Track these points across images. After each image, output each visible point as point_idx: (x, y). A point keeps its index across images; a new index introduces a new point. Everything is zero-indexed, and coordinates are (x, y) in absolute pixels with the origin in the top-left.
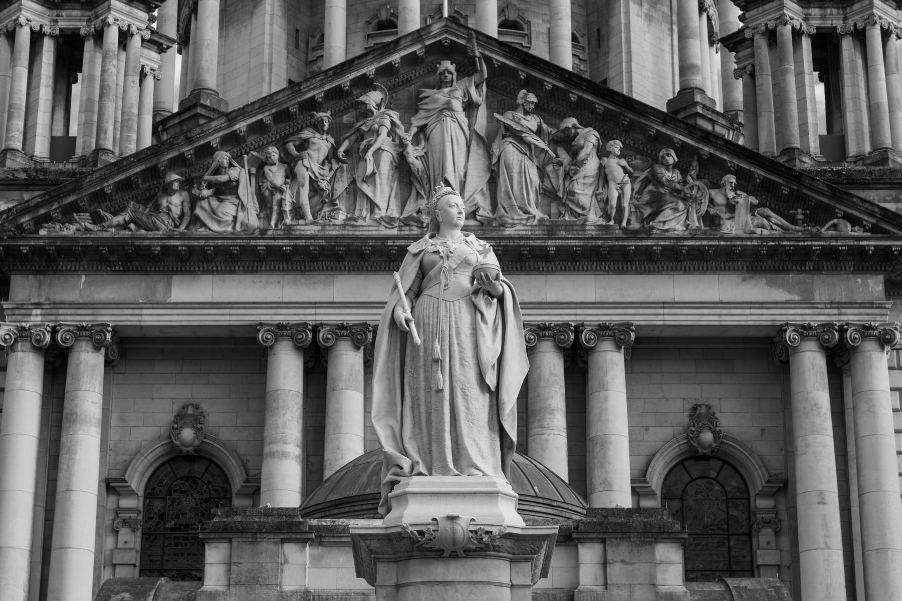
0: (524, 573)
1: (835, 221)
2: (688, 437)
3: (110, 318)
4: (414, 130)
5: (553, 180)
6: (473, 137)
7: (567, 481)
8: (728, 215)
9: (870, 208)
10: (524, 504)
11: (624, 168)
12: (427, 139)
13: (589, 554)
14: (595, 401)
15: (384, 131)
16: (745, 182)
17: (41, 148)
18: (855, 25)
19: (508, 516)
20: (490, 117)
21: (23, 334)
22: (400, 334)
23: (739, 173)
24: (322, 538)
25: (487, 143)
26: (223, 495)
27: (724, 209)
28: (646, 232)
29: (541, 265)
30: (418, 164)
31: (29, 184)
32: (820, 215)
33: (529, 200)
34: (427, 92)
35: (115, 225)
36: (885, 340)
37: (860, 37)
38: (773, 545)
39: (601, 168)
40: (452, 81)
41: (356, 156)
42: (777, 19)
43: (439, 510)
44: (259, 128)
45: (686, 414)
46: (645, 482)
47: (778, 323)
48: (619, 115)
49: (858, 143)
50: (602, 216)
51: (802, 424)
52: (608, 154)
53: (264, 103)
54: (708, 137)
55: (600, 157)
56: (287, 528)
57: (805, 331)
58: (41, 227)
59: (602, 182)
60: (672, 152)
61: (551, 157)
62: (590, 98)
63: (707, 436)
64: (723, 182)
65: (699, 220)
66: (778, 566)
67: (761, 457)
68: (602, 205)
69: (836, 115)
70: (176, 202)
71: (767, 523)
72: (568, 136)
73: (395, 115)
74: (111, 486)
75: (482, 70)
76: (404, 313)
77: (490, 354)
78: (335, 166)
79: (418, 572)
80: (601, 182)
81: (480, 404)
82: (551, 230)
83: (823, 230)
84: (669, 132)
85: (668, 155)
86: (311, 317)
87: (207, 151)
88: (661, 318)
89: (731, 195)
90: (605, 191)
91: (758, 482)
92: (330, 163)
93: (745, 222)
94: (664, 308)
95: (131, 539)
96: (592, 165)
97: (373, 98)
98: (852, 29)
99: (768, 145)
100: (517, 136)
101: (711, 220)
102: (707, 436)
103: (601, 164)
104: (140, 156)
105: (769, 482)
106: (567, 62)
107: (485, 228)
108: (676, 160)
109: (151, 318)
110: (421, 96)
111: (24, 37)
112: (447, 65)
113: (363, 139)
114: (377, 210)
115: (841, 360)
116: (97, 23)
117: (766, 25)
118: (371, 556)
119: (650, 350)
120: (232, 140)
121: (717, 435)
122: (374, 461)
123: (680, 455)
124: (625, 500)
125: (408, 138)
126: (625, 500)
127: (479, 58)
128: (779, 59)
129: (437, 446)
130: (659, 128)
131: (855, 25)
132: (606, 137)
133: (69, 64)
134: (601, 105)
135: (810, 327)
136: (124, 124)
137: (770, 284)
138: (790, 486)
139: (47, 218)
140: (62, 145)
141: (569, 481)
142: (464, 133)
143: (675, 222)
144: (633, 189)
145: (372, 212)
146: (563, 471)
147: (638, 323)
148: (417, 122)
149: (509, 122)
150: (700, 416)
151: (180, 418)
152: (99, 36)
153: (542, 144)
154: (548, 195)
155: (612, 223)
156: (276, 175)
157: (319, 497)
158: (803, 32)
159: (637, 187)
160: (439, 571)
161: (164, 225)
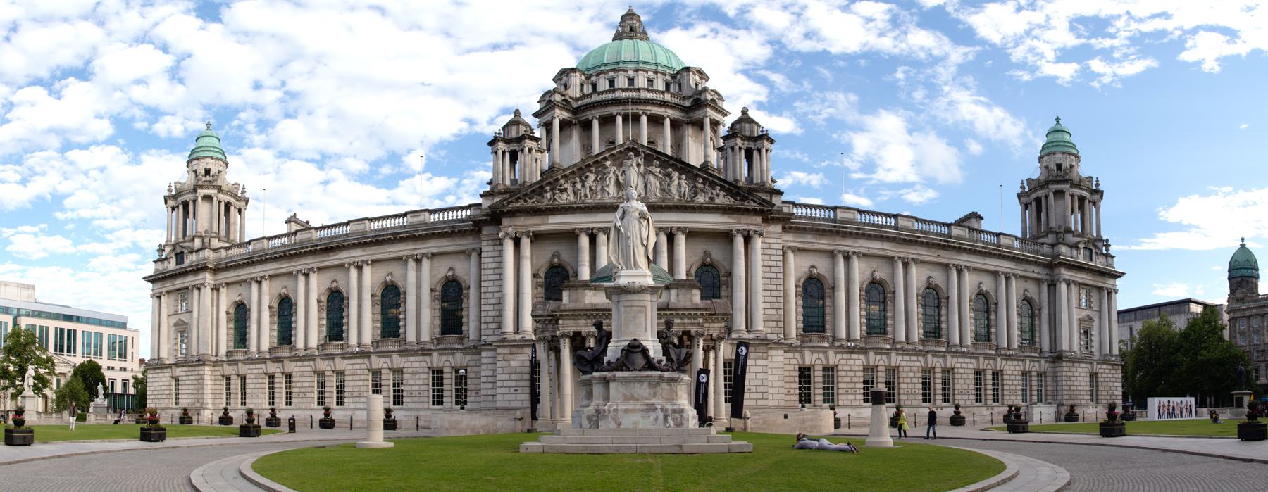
0: (655, 298)
3: (532, 229)
6: (639, 174)
9: (759, 198)
10: (655, 278)
13: (673, 292)
14: (676, 249)
16: (723, 188)
17: (508, 183)
19: (650, 282)
21: (507, 234)
22: (618, 230)
24: (596, 288)
25: (644, 176)
26: (567, 277)
28: (692, 201)
31: (505, 192)
32: (744, 199)
35: (531, 203)
36: (761, 235)
37: (759, 151)
41: (603, 179)
43: (630, 280)
44: (573, 173)
48: (685, 168)
49: (757, 180)
51: (735, 257)
53: (574, 166)
54: (712, 175)
56: (586, 286)
57: (738, 231)
59: (679, 186)
62: (677, 163)
70: (549, 195)
74: (535, 276)
76: (619, 224)
77: (645, 236)
79: (624, 297)
81: (642, 250)
82: (663, 201)
86: (591, 226)
87: (557, 180)
91: (722, 273)
93: (722, 199)
95: (542, 290)
96: (676, 182)
97: (608, 163)
99: (730, 179)
100: (653, 174)
101: (712, 199)
104: (537, 183)
106: (669, 153)
107: (643, 200)
109: (543, 228)
111: (500, 153)
115: (748, 239)
118: (610, 293)
119: (691, 235)
120: (565, 177)
122: (611, 266)
124: (684, 277)
126: (684, 277)
128: (734, 155)
129: (630, 263)
133: (514, 158)
136: (532, 173)
140: (514, 181)
143: (701, 199)
146: (666, 268)
150: (707, 254)
151: (553, 256)
152: (522, 150)
154: (663, 190)
156: (579, 186)
157: (595, 276)
160: (630, 297)
161: (546, 201)
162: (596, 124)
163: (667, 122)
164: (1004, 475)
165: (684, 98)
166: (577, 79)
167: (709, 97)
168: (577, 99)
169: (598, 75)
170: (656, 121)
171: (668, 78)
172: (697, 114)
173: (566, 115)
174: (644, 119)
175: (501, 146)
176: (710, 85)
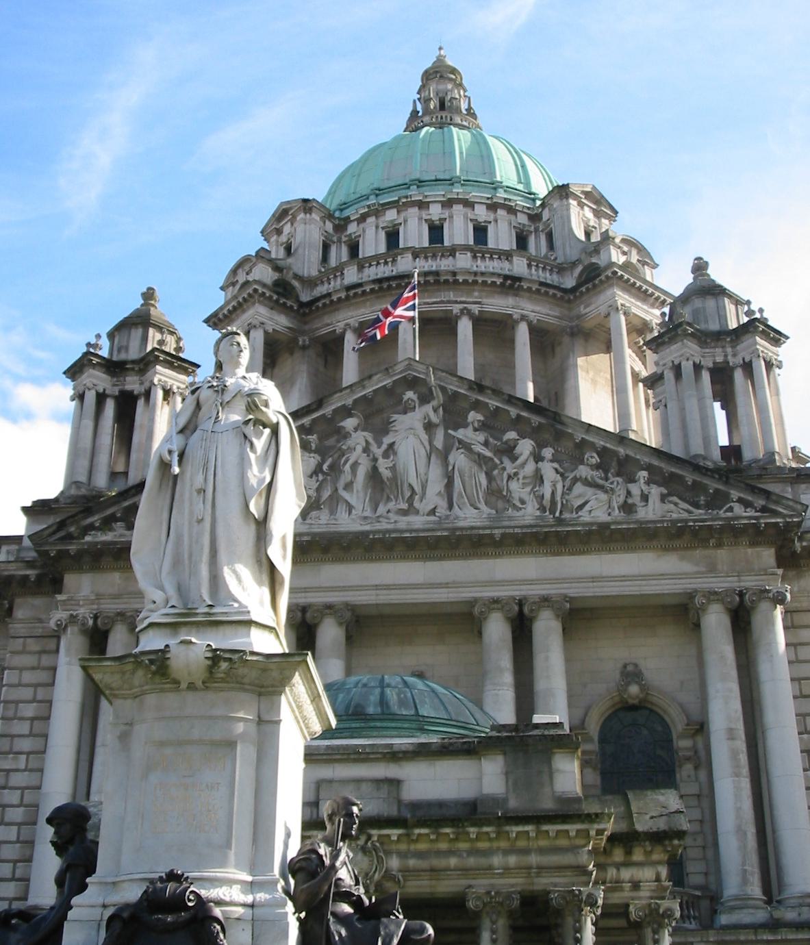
1: (732, 504)
2: (619, 690)
4: (384, 447)
5: (499, 482)
8: (643, 504)
11: (556, 470)
12: (395, 454)
15: (359, 449)
18: (744, 359)
20: (447, 435)
21: (73, 619)
23: (649, 468)
29: (490, 550)
30: (386, 473)
32: (718, 501)
33: (478, 498)
34: (395, 417)
37: (748, 368)
38: (693, 778)
39: (538, 470)
40: (415, 407)
46: (584, 729)
47: (689, 591)
50: (538, 509)
55: (537, 463)
57: (712, 595)
58: (86, 534)
60: (595, 455)
61: (496, 464)
64: (637, 477)
65: (619, 508)
66: (699, 796)
67: (681, 705)
68: (539, 500)
69: (734, 430)
71: (688, 759)
72: (510, 446)
73: (369, 436)
75: (438, 397)
78: (321, 477)
80: (538, 482)
83: (722, 511)
84: (591, 439)
85: (592, 457)
88: (592, 590)
92: (317, 476)
94: (593, 582)
96: (530, 468)
97: (350, 423)
98: (742, 362)
100: (466, 446)
101: (627, 508)
105: (688, 725)
108: (599, 461)
110: (391, 420)
112: (410, 395)
113: (344, 455)
114: (353, 511)
115: (742, 621)
116: (147, 385)
117: (673, 362)
119: (579, 617)
121: (643, 688)
123: (614, 706)
125: (378, 452)
127: (435, 387)
130: (584, 436)
131: (744, 359)
132: (540, 445)
135: (716, 593)
137: (682, 558)
138: (705, 727)
139: (91, 527)
142: (425, 447)
144: (564, 486)
145: (350, 513)
147: (572, 595)
148: (387, 440)
149: (461, 437)
152: (148, 394)
153: (488, 454)
155: (547, 513)
158: (702, 367)
159: (568, 483)
162: (350, 340)
163: (522, 334)
164: (584, 731)
165: (561, 269)
166: (308, 232)
167: (617, 257)
168: (310, 283)
169: (363, 219)
170: (494, 331)
171: (522, 219)
172: (593, 309)
173: (281, 322)
174: (465, 328)
175: (97, 379)
176: (619, 230)
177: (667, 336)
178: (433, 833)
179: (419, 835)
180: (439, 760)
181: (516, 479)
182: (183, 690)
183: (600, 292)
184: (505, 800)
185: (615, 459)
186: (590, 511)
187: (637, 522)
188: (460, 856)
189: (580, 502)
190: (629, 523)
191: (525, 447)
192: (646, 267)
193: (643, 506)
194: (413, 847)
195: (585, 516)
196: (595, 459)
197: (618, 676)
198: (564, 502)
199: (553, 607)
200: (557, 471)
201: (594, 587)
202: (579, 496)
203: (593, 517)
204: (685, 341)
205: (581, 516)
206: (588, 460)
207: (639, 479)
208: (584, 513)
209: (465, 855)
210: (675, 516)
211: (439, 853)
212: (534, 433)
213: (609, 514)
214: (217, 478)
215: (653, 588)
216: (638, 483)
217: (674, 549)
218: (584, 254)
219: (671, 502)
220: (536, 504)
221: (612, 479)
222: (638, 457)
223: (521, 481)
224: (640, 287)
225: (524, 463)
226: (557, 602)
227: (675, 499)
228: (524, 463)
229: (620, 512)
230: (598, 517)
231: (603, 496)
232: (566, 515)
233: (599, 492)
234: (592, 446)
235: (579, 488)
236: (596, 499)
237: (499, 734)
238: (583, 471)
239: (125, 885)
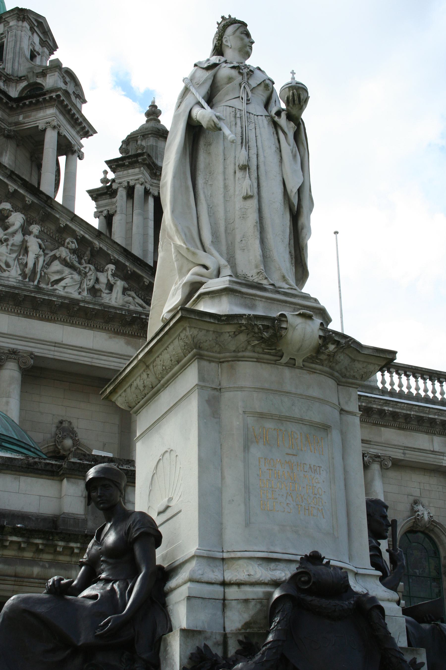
7: (18, 423)
8: (107, 291)
23: (116, 263)
27: (105, 286)
39: (24, 242)
42: (136, 180)
45: (54, 425)
50: (20, 275)
52: (30, 233)
55: (24, 235)
63: (68, 442)
65: (87, 290)
72: (3, 215)
80: (22, 252)
84: (74, 227)
85: (72, 242)
88: (52, 353)
89: (111, 278)
90: (25, 258)
94: (55, 346)
96: (18, 238)
102: (68, 442)
103: (24, 239)
108: (77, 247)
117: (128, 183)
130: (68, 223)
132: (28, 222)
134: (29, 198)
137: (128, 343)
141: (20, 421)
144: (44, 261)
147: (36, 354)
155: (27, 280)
158: (150, 193)
159: (48, 258)
177: (128, 160)
178: (24, 542)
179: (12, 542)
180: (24, 476)
181: (5, 244)
182: (281, 364)
183: (41, 109)
184: (85, 521)
185: (89, 249)
186: (65, 287)
187: (101, 305)
188: (43, 567)
189: (57, 277)
190: (95, 304)
191: (17, 219)
192: (78, 99)
193: (107, 294)
194: (21, 554)
195: (59, 289)
196: (74, 246)
197: (54, 430)
198: (43, 274)
199: (19, 359)
200: (40, 247)
201: (54, 351)
202: (58, 272)
203: (67, 292)
204: (142, 168)
205: (56, 289)
206: (68, 243)
207: (107, 271)
208: (59, 287)
209: (47, 565)
210: (132, 307)
211: (23, 561)
212: (25, 209)
213: (80, 293)
214: (259, 158)
215: (102, 362)
216: (105, 274)
217: (124, 334)
218: (31, 73)
219: (129, 295)
220: (19, 269)
221: (85, 265)
222: (109, 252)
223: (9, 247)
224: (74, 114)
225: (14, 233)
226: (23, 357)
227: (133, 294)
228: (14, 233)
229: (88, 294)
230: (71, 293)
231: (76, 277)
232: (42, 285)
233: (74, 273)
234: (73, 233)
235: (56, 266)
236: (72, 278)
237: (81, 462)
238: (63, 252)
239: (241, 562)
